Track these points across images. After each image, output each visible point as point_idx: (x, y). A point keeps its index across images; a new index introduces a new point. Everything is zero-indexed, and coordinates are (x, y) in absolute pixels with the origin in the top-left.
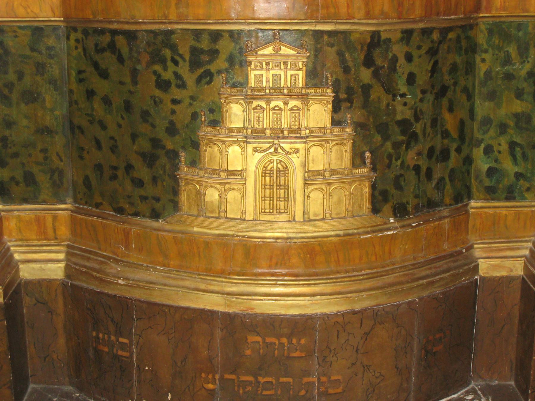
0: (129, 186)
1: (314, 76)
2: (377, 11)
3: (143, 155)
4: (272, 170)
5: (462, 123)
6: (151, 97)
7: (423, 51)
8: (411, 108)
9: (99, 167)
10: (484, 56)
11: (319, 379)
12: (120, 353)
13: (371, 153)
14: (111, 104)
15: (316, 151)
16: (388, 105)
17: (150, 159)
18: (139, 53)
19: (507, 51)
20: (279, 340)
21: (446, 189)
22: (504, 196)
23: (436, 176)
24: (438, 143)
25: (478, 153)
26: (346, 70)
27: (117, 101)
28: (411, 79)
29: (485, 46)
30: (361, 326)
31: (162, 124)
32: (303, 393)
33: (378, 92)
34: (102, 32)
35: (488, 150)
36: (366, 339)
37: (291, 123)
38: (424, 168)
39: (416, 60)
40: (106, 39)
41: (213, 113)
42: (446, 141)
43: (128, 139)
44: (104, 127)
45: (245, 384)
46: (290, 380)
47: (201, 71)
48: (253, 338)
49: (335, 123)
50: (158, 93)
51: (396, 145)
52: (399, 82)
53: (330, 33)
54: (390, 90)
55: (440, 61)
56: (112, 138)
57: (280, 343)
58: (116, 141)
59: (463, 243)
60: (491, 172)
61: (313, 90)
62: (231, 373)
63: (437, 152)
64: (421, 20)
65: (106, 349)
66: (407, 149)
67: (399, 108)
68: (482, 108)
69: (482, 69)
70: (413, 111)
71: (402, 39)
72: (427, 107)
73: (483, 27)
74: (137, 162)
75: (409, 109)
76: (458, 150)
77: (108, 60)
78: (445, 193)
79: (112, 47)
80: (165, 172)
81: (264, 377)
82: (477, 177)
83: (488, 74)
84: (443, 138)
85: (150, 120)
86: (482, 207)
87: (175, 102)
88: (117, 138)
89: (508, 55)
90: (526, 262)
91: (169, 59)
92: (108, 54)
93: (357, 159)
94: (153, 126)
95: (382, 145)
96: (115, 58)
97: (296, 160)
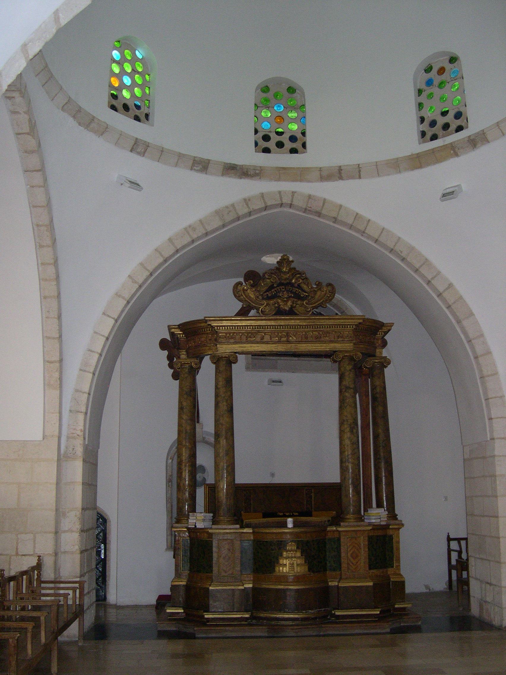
1: (298, 548)
15: (298, 560)
25: (328, 562)
35: (330, 562)
60: (330, 566)
69: (327, 547)
93: (305, 562)
97: (295, 562)
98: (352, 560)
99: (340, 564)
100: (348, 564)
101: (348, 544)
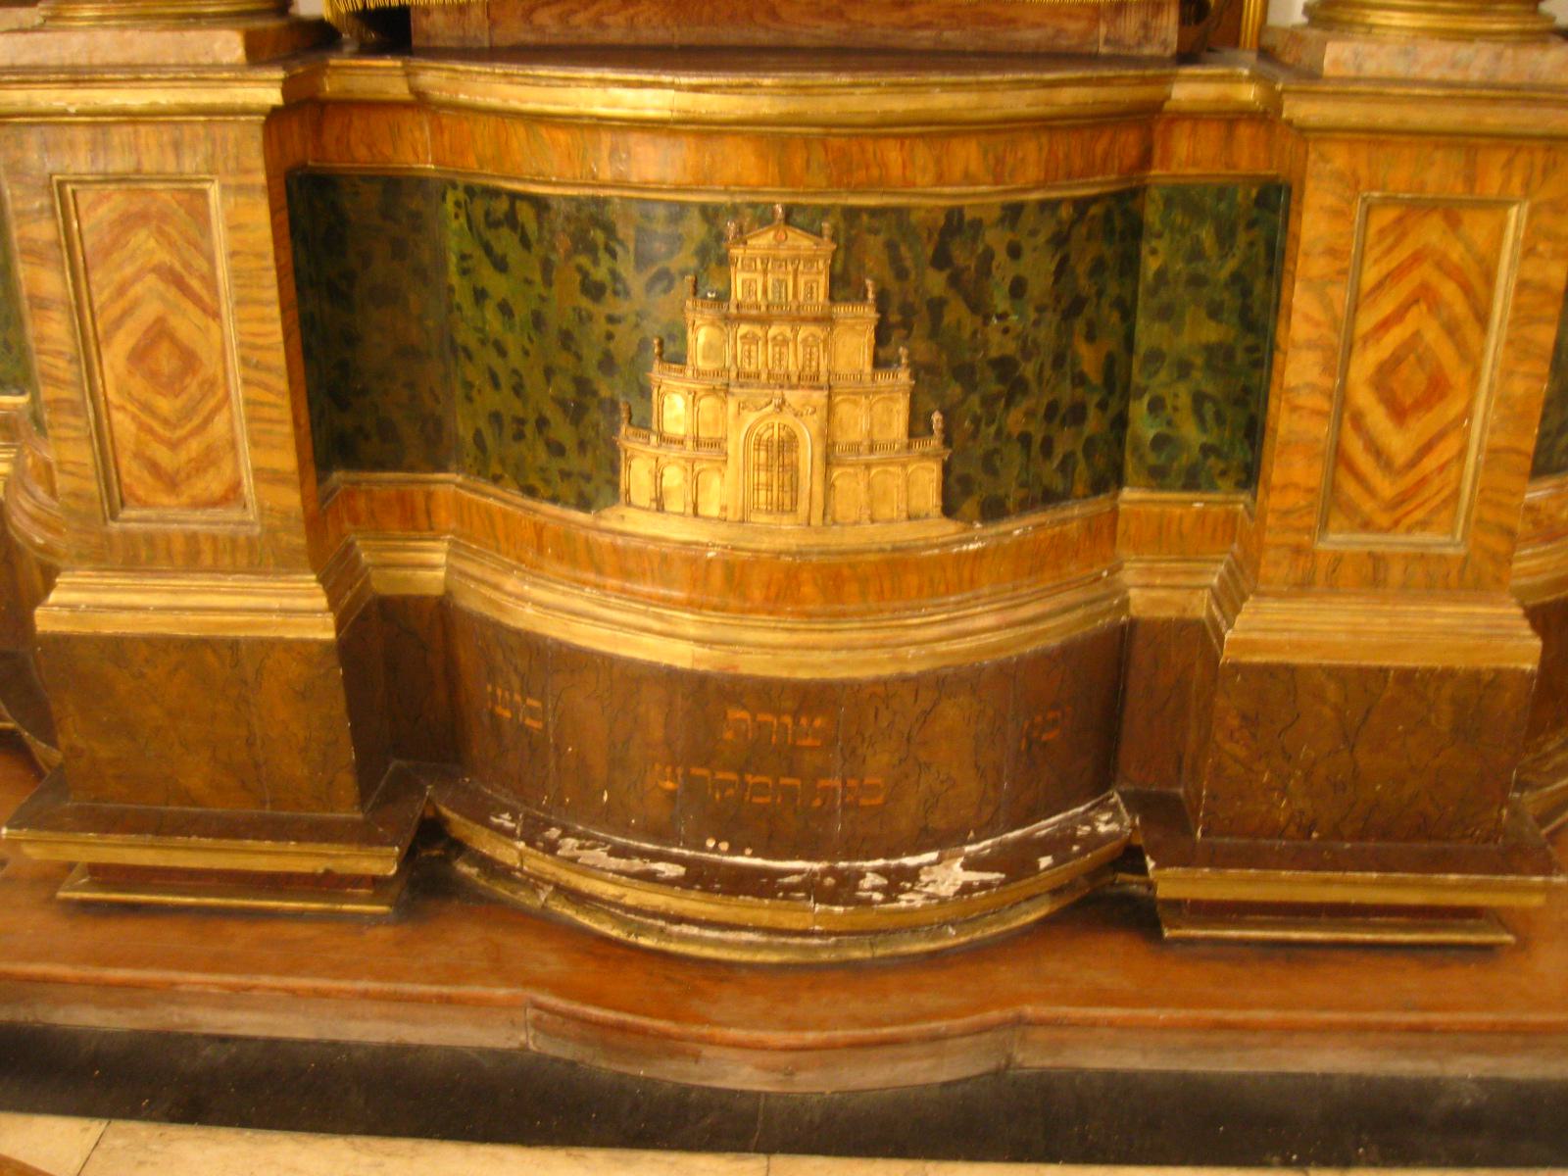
0: (543, 454)
1: (842, 285)
2: (957, 172)
3: (561, 403)
4: (770, 440)
5: (1110, 363)
6: (574, 309)
7: (1042, 239)
8: (1018, 337)
9: (496, 418)
10: (1154, 243)
11: (844, 783)
12: (528, 722)
13: (945, 413)
14: (513, 316)
16: (974, 333)
17: (576, 413)
18: (553, 232)
19: (1197, 236)
20: (779, 719)
21: (1077, 471)
22: (1180, 483)
23: (1059, 451)
24: (1066, 393)
25: (1139, 409)
26: (901, 274)
27: (522, 313)
28: (1018, 289)
29: (1158, 226)
30: (916, 701)
31: (592, 357)
32: (817, 803)
33: (957, 312)
34: (495, 193)
35: (1156, 405)
36: (925, 722)
37: (804, 363)
38: (1038, 439)
39: (1028, 256)
40: (502, 206)
41: (674, 341)
42: (1079, 391)
43: (538, 375)
44: (502, 352)
45: (723, 786)
46: (797, 782)
47: (654, 270)
48: (737, 714)
49: (879, 363)
50: (585, 303)
51: (988, 402)
52: (995, 293)
53: (875, 212)
54: (978, 306)
55: (1073, 256)
56: (515, 372)
57: (780, 724)
58: (521, 377)
59: (1105, 560)
60: (1160, 442)
61: (840, 310)
62: (701, 766)
63: (1062, 411)
64: (1038, 187)
65: (507, 714)
66: (1008, 405)
67: (995, 337)
68: (1149, 333)
69: (1151, 265)
70: (1020, 342)
71: (1002, 220)
72: (1045, 335)
73: (1155, 193)
74: (552, 413)
75: (1013, 339)
76: (1102, 406)
77: (505, 242)
78: (1076, 477)
79: (512, 220)
80: (597, 433)
81: (754, 775)
82: (1135, 449)
83: (1161, 275)
84: (1074, 385)
85: (574, 348)
86: (1141, 502)
87: (611, 319)
88: (523, 372)
89: (1197, 240)
90: (1233, 565)
91: (601, 247)
92: (505, 231)
94: (579, 357)
95: (963, 401)
96: (516, 238)
98: (1377, 417)
99: (1254, 431)
100: (1339, 457)
101: (1370, 276)
